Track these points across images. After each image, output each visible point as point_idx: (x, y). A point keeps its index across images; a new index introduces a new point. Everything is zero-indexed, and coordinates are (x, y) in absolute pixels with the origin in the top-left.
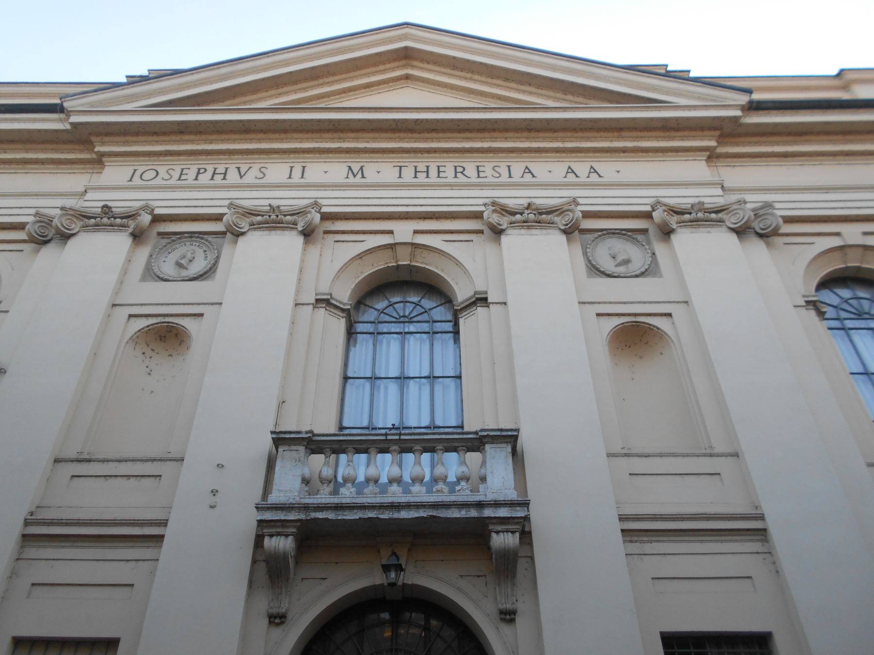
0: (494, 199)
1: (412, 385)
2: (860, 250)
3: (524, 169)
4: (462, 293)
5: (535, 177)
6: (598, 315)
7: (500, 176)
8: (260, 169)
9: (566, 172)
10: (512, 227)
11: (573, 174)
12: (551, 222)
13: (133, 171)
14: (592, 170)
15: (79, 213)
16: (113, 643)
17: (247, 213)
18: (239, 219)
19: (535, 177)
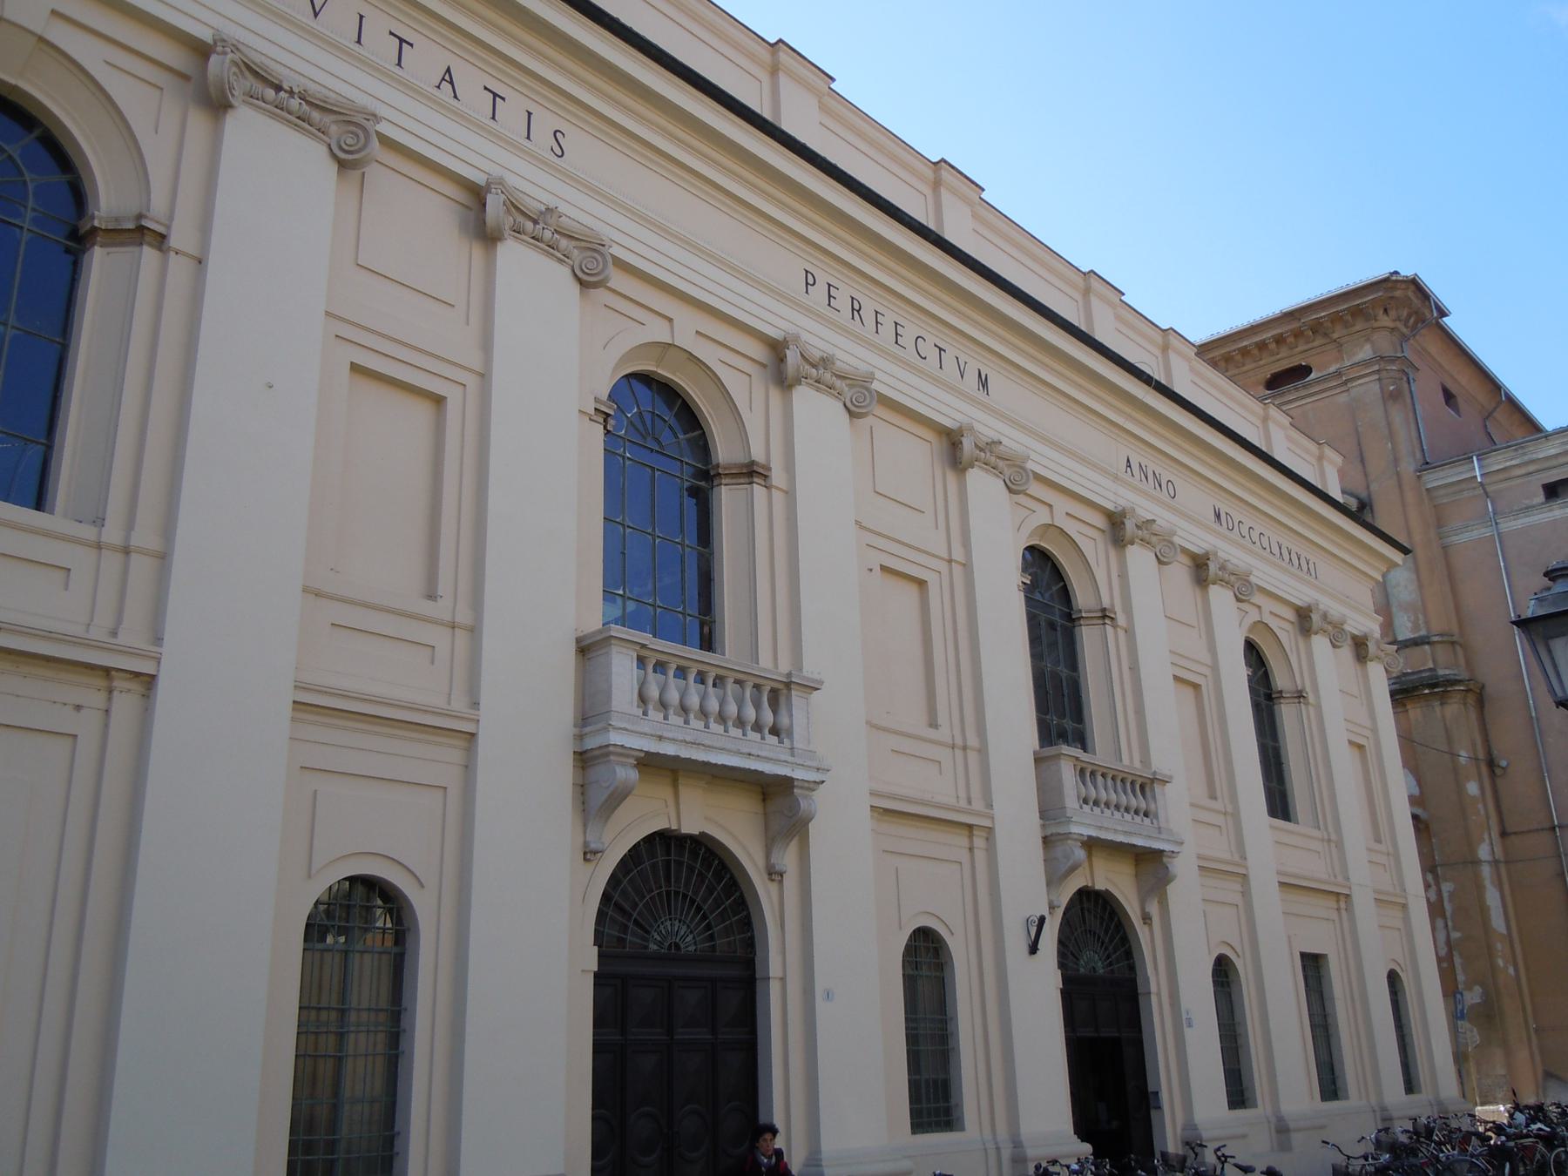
0: (801, 331)
1: (134, 542)
2: (686, 356)
3: (443, 73)
4: (724, 452)
5: (401, 66)
6: (355, 368)
7: (559, 157)
8: (556, 132)
9: (441, 78)
10: (548, 252)
11: (450, 85)
12: (323, 129)
13: (486, 91)
14: (447, 77)
15: (246, 61)
16: (910, 1173)
17: (511, 202)
18: (237, 71)
19: (401, 66)
